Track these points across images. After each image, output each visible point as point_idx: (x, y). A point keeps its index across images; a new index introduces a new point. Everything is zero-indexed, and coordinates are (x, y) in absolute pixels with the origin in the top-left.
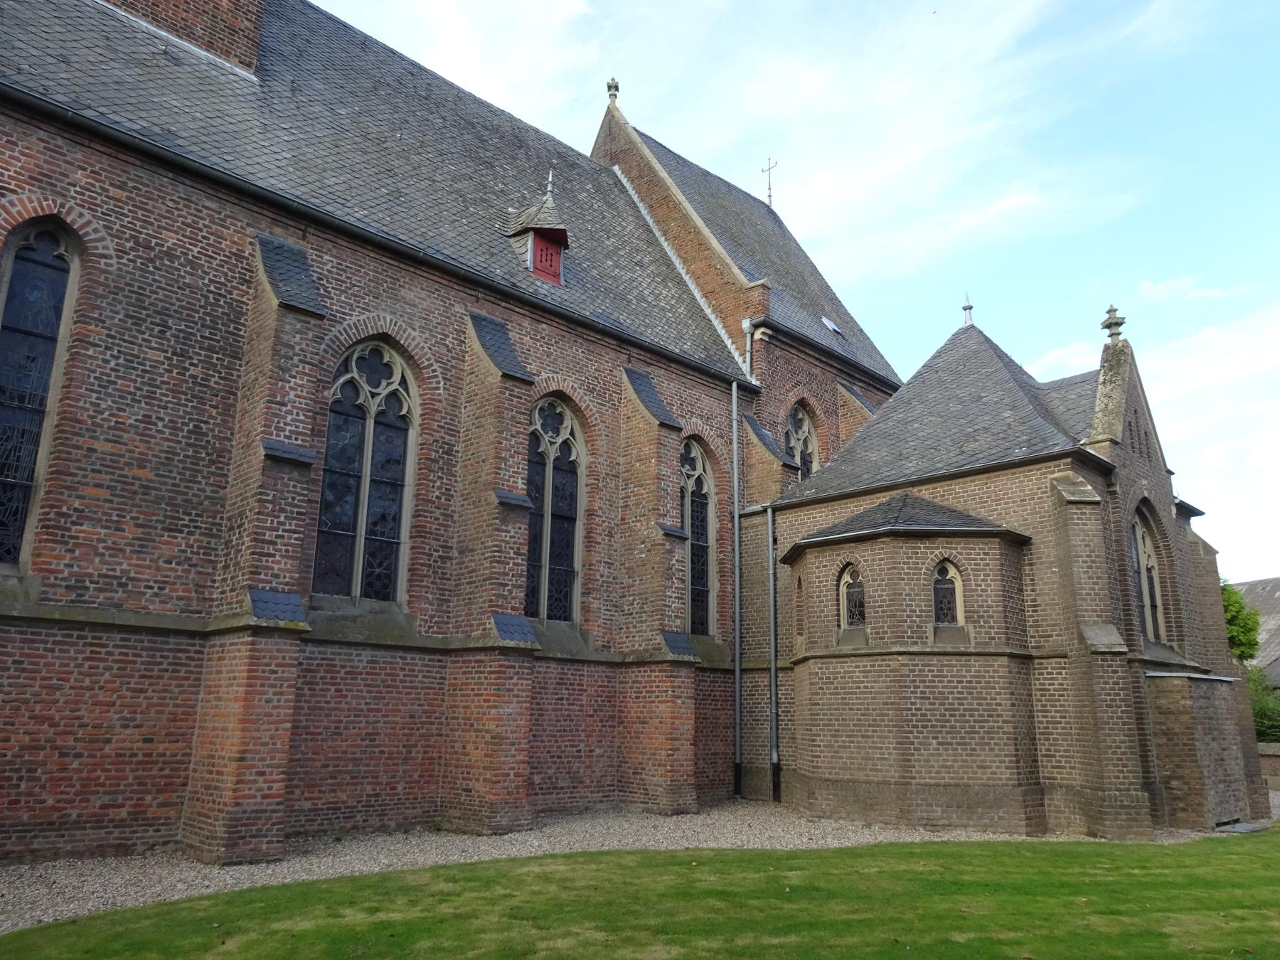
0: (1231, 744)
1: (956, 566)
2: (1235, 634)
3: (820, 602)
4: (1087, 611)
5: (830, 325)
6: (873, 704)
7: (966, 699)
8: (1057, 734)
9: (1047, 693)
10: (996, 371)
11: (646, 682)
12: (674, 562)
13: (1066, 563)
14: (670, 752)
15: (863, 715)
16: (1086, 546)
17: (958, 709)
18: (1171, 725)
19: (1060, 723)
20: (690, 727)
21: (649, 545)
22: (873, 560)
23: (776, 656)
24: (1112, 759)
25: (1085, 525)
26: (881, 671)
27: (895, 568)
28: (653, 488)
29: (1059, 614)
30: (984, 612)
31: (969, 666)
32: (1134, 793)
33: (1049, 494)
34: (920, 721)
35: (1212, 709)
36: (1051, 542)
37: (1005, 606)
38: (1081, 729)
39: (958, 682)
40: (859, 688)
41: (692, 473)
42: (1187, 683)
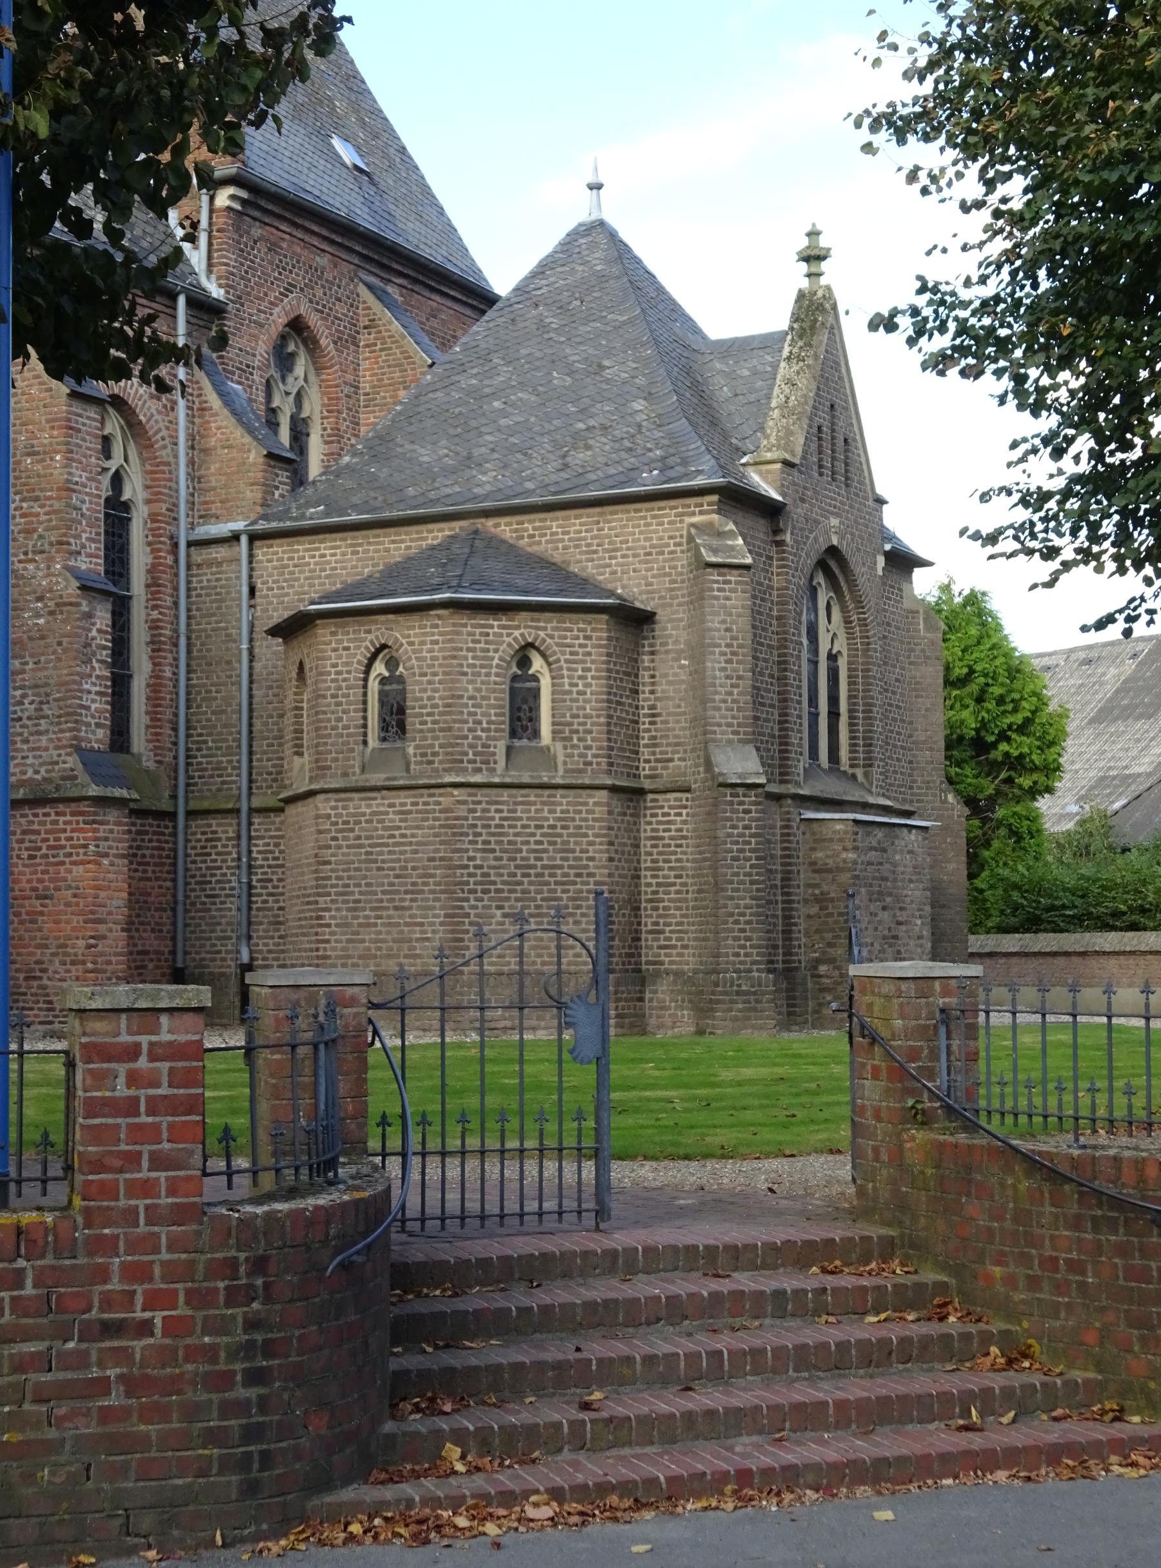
0: (913, 916)
1: (544, 656)
2: (1026, 750)
3: (339, 704)
4: (719, 725)
5: (347, 153)
6: (413, 860)
7: (545, 851)
8: (670, 900)
9: (661, 843)
10: (630, 321)
11: (47, 832)
12: (94, 633)
13: (698, 652)
14: (92, 941)
15: (397, 876)
16: (727, 630)
17: (535, 867)
18: (825, 888)
19: (674, 884)
20: (121, 903)
21: (51, 604)
22: (423, 643)
23: (250, 788)
24: (733, 931)
25: (727, 598)
26: (427, 812)
27: (454, 657)
28: (57, 505)
29: (684, 729)
30: (580, 724)
31: (553, 803)
32: (756, 974)
33: (685, 547)
34: (480, 883)
35: (887, 866)
36: (681, 620)
37: (610, 717)
38: (699, 891)
39: (537, 827)
40: (393, 836)
41: (107, 464)
42: (850, 827)
